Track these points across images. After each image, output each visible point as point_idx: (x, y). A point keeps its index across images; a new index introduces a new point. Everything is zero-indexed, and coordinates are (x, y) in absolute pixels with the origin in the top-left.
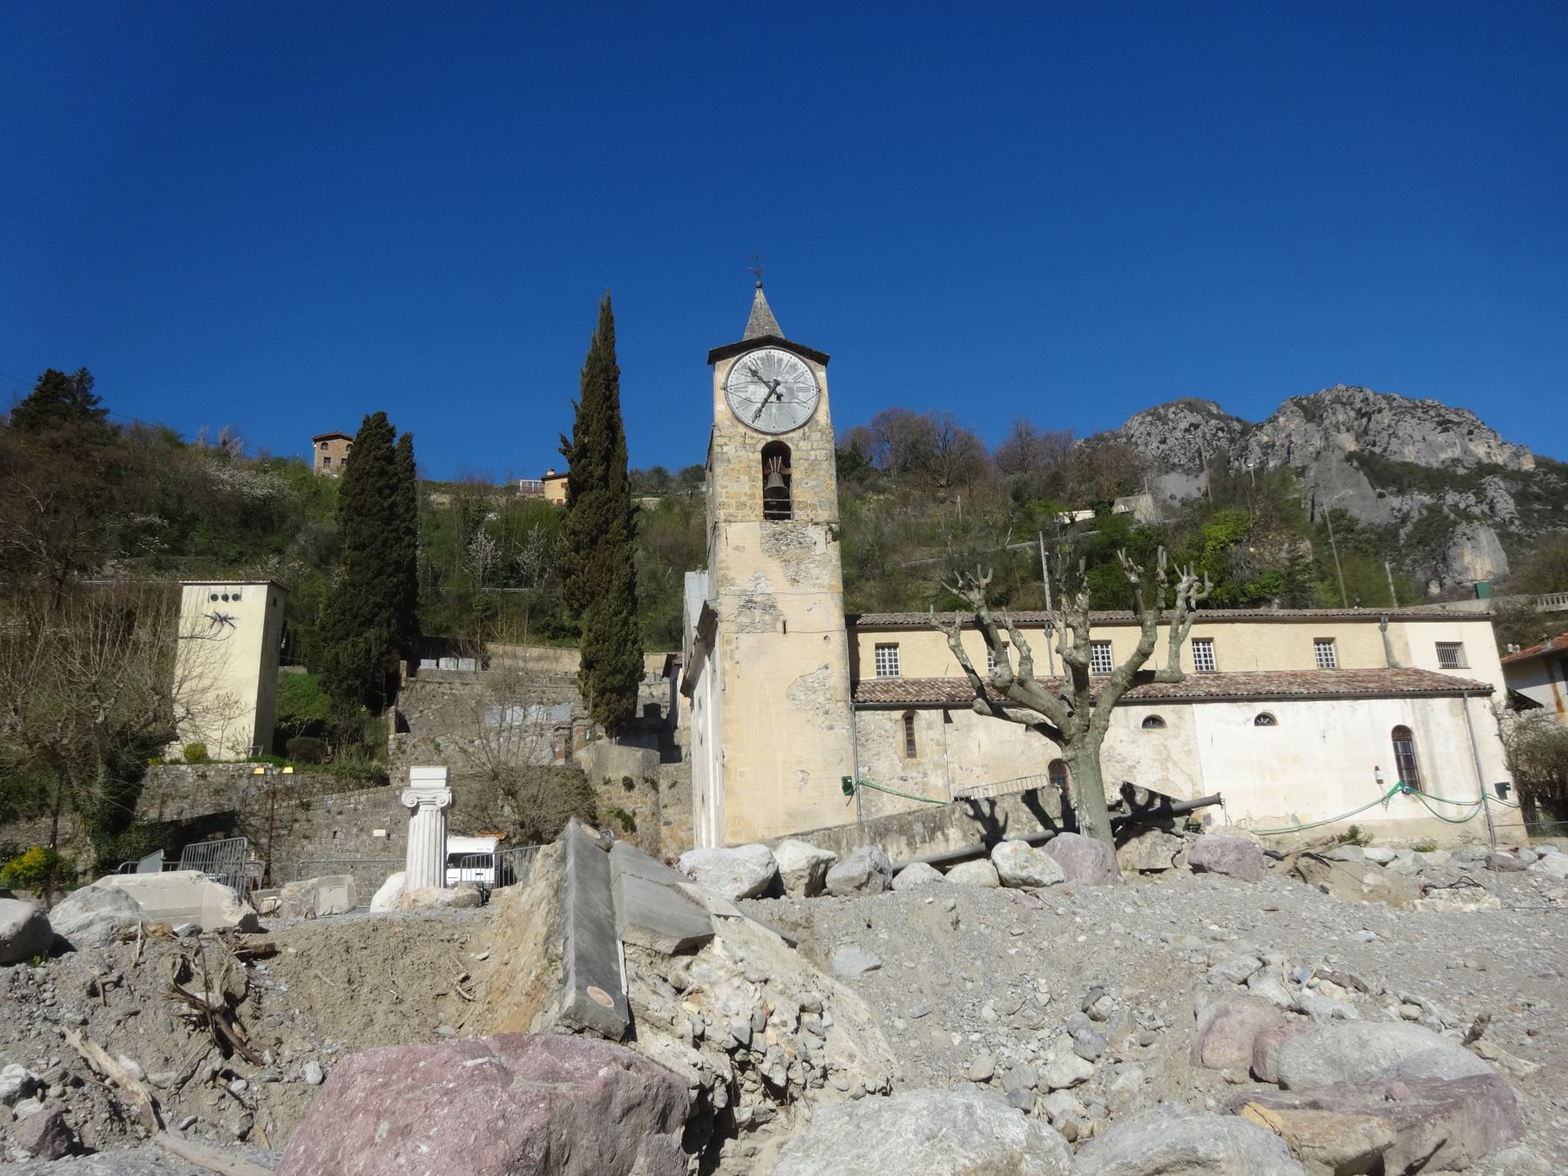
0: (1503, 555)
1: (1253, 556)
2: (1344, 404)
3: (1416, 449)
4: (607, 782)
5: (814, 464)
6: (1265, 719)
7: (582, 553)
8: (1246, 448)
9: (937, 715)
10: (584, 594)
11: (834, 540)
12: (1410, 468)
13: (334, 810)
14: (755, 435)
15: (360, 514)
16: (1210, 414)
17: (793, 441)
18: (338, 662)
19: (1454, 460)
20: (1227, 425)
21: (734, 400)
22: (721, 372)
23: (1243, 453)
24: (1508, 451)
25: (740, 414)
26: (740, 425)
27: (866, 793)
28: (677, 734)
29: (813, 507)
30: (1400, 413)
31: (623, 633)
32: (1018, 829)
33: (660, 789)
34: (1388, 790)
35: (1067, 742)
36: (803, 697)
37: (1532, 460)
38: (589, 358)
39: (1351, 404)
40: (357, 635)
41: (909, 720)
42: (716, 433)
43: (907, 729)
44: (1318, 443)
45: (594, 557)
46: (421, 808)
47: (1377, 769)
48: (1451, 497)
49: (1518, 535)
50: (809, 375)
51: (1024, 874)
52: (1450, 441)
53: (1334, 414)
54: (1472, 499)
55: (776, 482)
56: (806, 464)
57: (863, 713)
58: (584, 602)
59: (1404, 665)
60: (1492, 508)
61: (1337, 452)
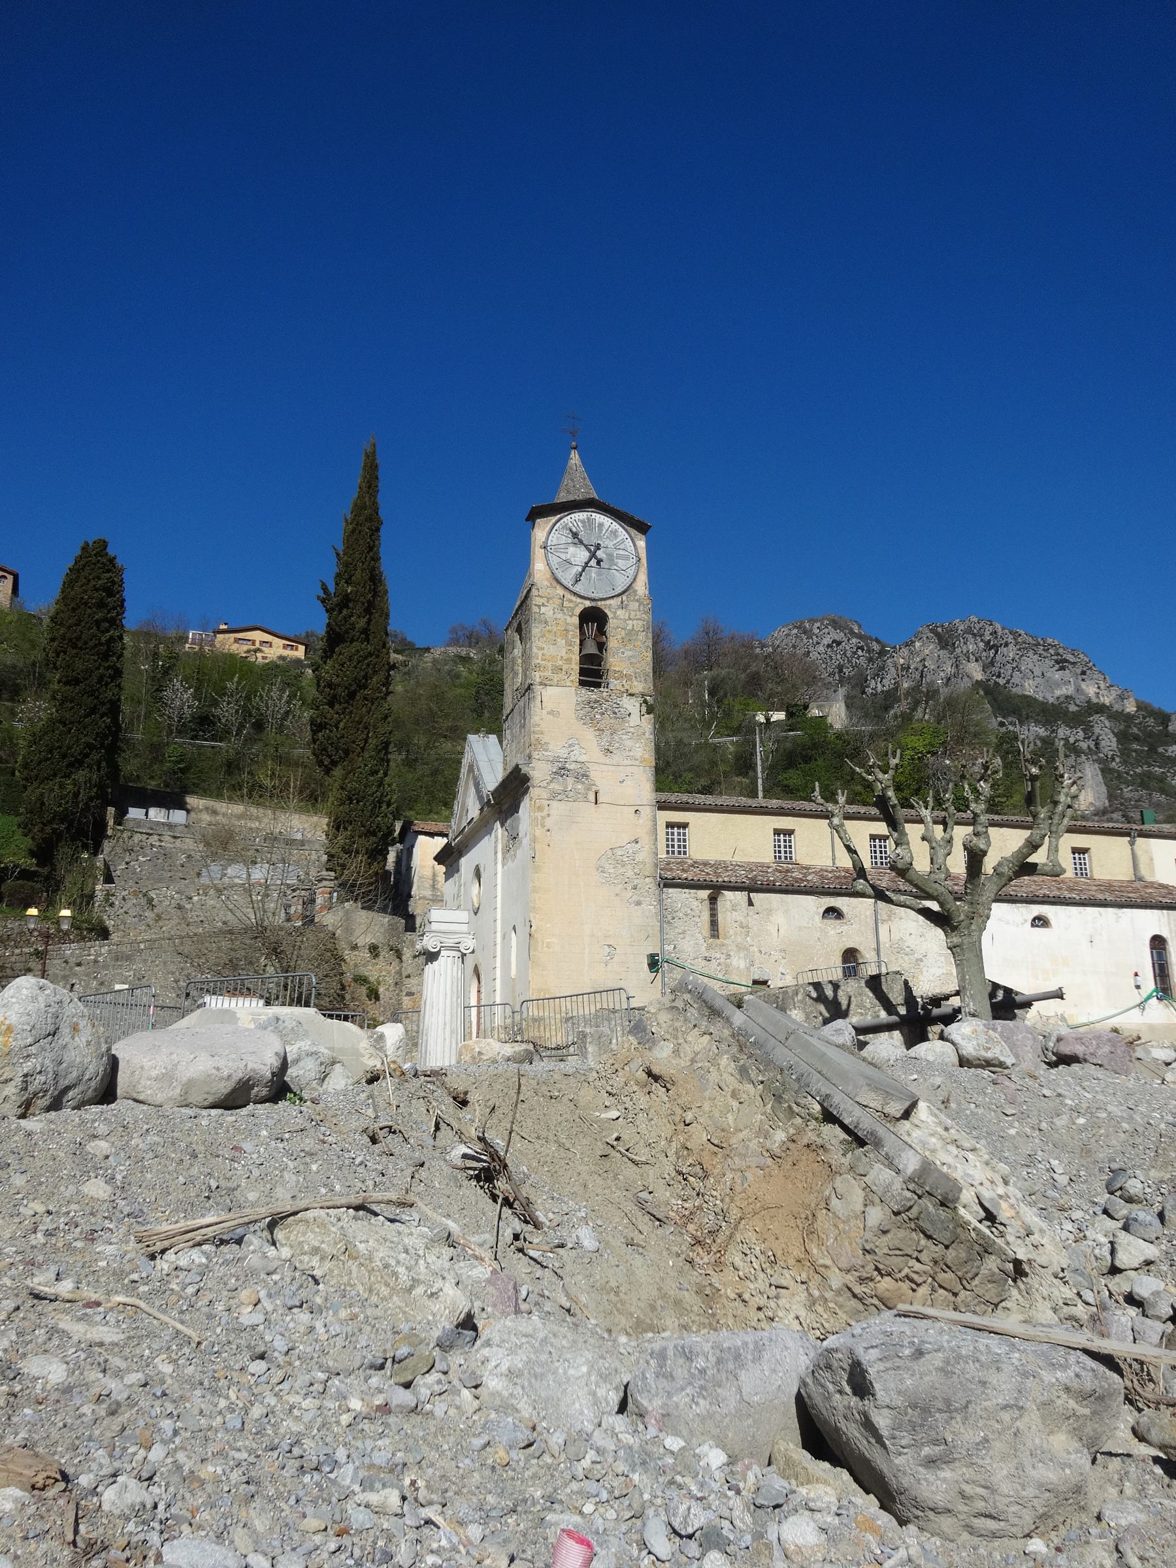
0: (1104, 789)
1: (949, 768)
2: (974, 635)
3: (1035, 683)
4: (355, 947)
5: (631, 634)
6: (1040, 922)
7: (337, 706)
8: (882, 668)
9: (740, 897)
10: (337, 749)
11: (648, 713)
12: (1029, 701)
13: (73, 960)
14: (574, 598)
15: (75, 646)
16: (852, 632)
17: (610, 608)
18: (43, 804)
19: (1067, 697)
20: (867, 645)
21: (554, 560)
22: (541, 531)
23: (880, 673)
24: (1114, 693)
25: (559, 575)
26: (558, 587)
27: (671, 971)
28: (411, 903)
29: (628, 678)
30: (1024, 648)
31: (378, 794)
32: (862, 1014)
33: (404, 958)
34: (1145, 996)
35: (954, 929)
36: (612, 871)
37: (1134, 703)
38: (356, 505)
39: (981, 636)
40: (65, 776)
41: (713, 900)
42: (534, 592)
43: (711, 909)
44: (949, 669)
45: (351, 712)
46: (443, 953)
47: (1136, 975)
48: (1063, 731)
49: (1118, 771)
50: (629, 543)
51: (989, 1055)
52: (1065, 679)
53: (965, 643)
54: (1081, 734)
55: (591, 649)
56: (623, 633)
57: (671, 890)
58: (336, 758)
59: (1149, 878)
60: (1097, 745)
61: (966, 679)
